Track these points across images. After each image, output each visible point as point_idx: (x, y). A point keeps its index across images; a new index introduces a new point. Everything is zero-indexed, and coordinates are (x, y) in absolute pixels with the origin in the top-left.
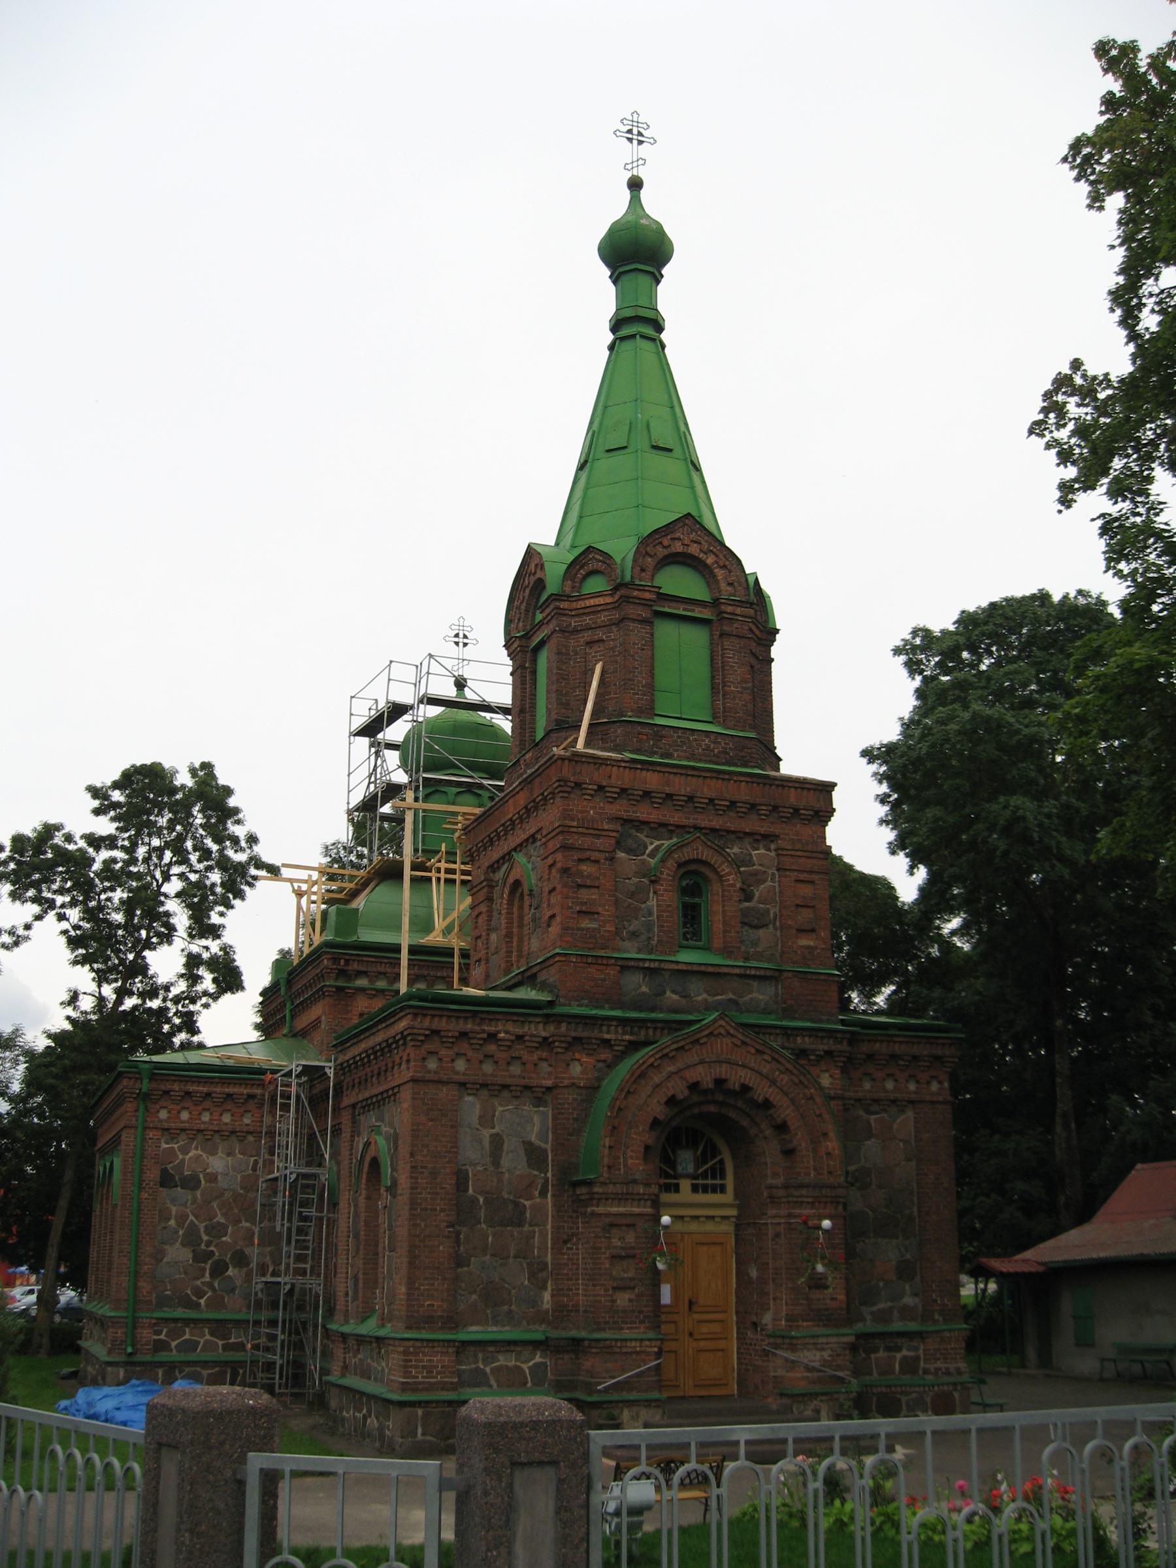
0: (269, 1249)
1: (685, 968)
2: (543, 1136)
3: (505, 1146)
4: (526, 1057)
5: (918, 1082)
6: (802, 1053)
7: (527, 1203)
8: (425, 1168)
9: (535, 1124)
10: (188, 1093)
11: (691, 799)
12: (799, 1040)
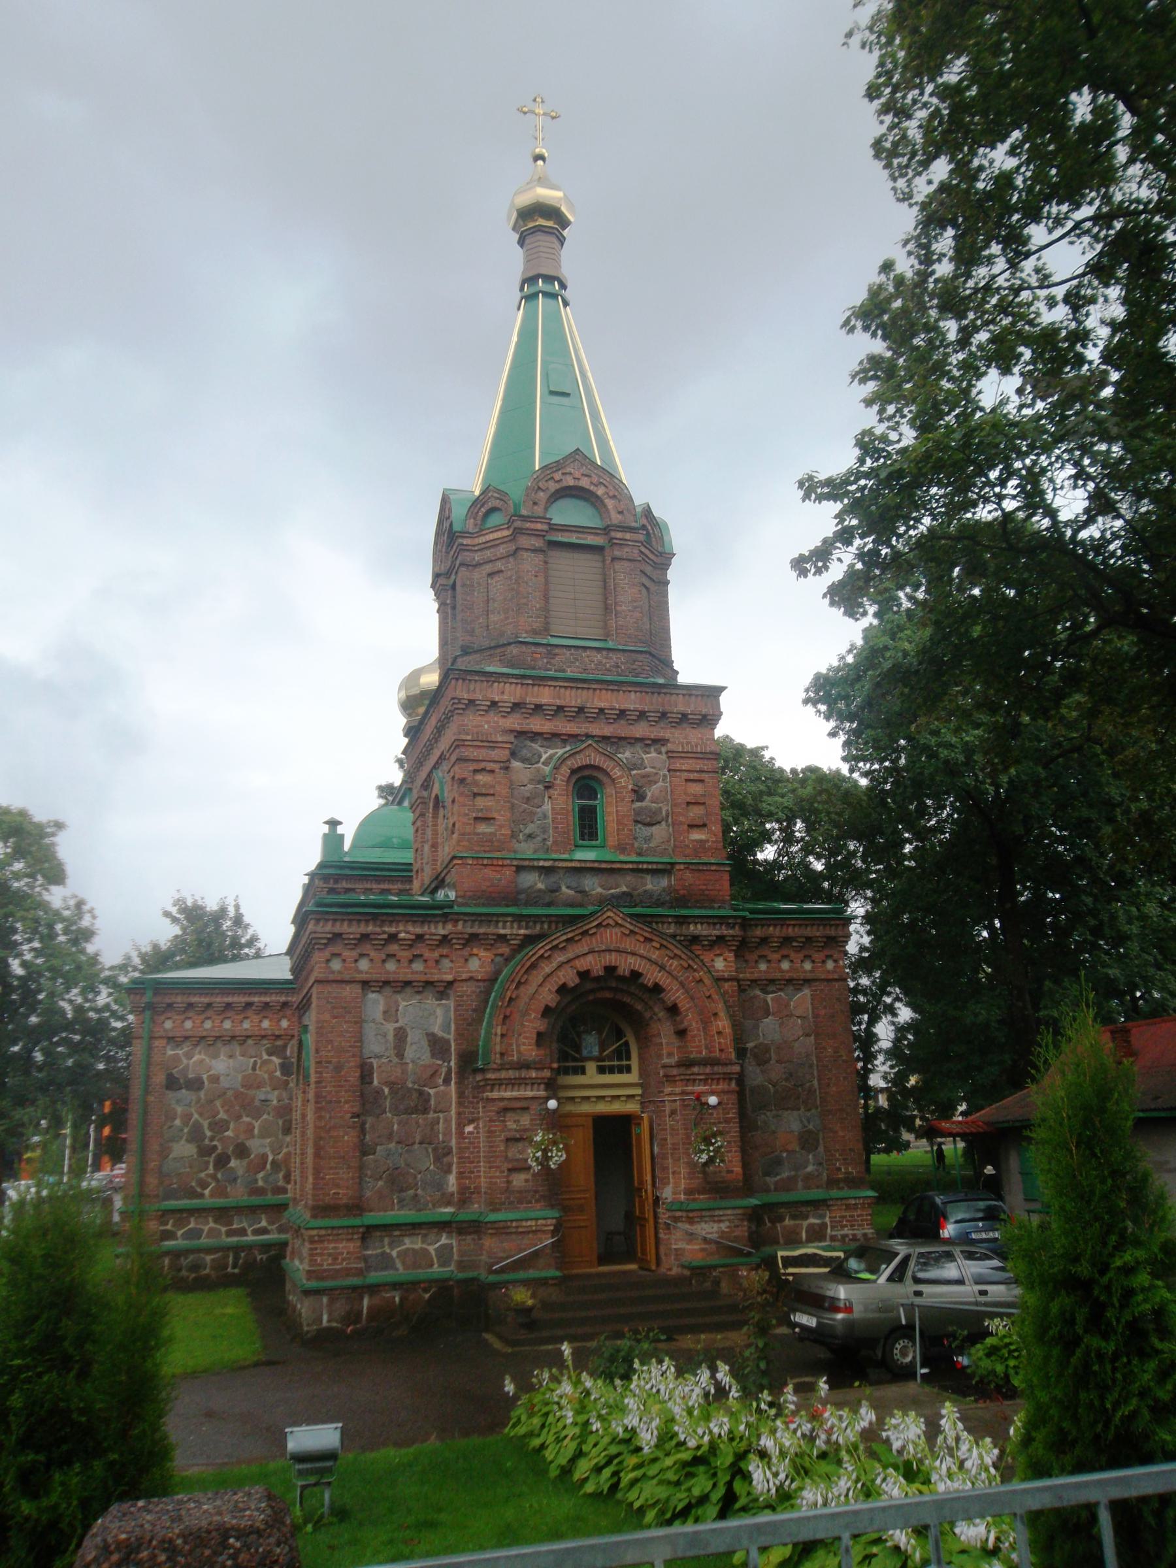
0: (268, 1140)
1: (578, 865)
2: (446, 1027)
3: (409, 1039)
4: (427, 954)
5: (813, 962)
6: (695, 939)
7: (432, 1091)
8: (329, 1062)
9: (438, 1016)
10: (191, 1005)
11: (581, 710)
12: (692, 927)
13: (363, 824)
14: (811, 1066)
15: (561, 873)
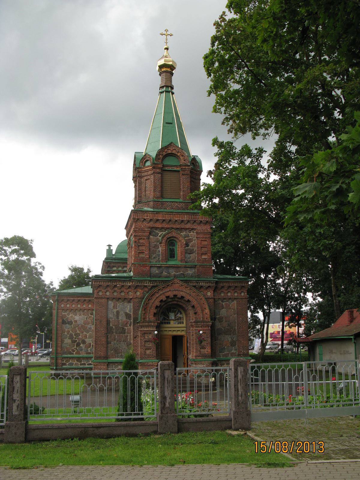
6: (202, 287)
11: (170, 220)
13: (119, 246)
14: (235, 323)
15: (164, 268)
